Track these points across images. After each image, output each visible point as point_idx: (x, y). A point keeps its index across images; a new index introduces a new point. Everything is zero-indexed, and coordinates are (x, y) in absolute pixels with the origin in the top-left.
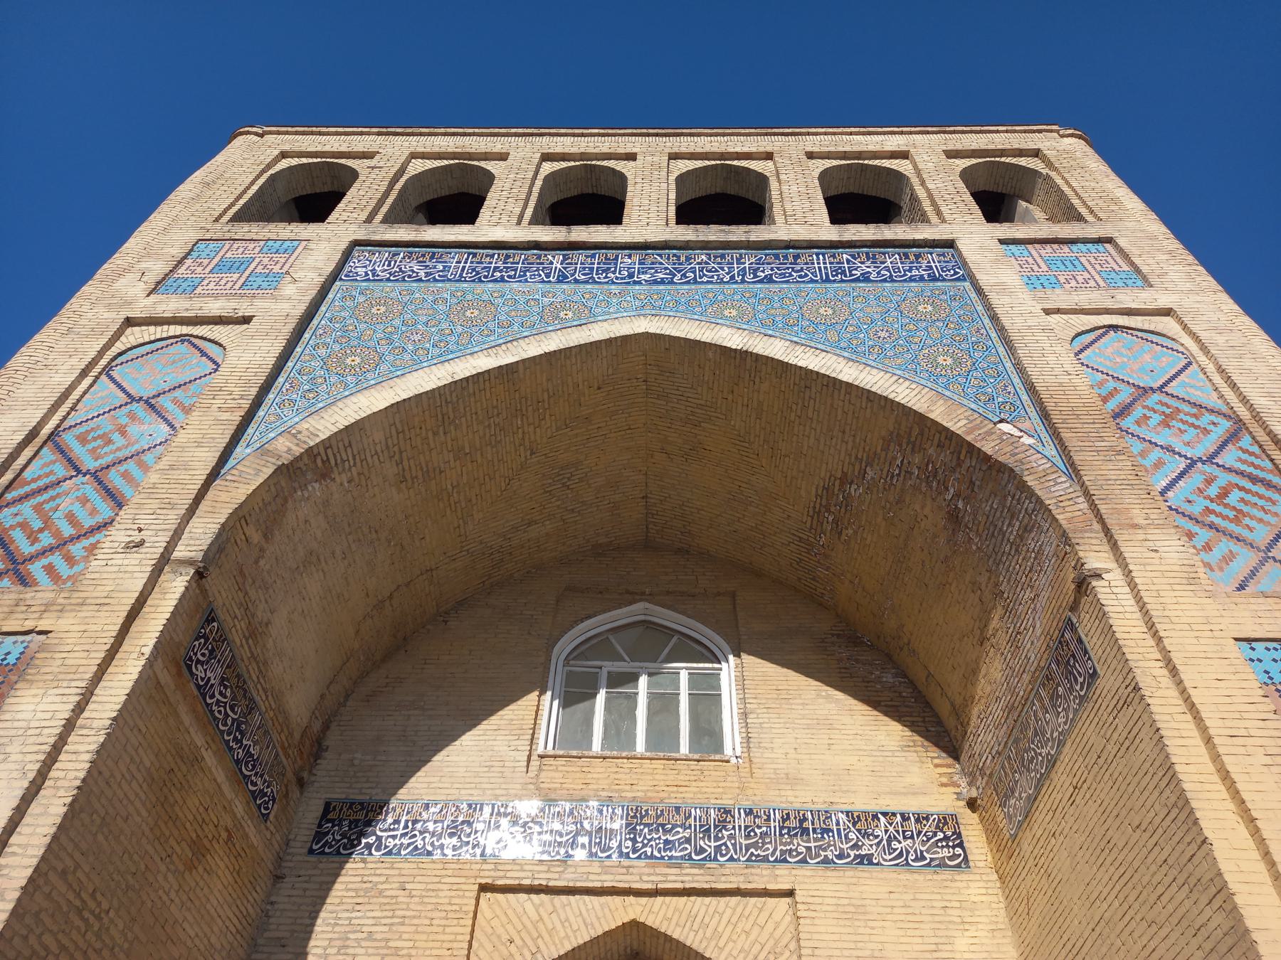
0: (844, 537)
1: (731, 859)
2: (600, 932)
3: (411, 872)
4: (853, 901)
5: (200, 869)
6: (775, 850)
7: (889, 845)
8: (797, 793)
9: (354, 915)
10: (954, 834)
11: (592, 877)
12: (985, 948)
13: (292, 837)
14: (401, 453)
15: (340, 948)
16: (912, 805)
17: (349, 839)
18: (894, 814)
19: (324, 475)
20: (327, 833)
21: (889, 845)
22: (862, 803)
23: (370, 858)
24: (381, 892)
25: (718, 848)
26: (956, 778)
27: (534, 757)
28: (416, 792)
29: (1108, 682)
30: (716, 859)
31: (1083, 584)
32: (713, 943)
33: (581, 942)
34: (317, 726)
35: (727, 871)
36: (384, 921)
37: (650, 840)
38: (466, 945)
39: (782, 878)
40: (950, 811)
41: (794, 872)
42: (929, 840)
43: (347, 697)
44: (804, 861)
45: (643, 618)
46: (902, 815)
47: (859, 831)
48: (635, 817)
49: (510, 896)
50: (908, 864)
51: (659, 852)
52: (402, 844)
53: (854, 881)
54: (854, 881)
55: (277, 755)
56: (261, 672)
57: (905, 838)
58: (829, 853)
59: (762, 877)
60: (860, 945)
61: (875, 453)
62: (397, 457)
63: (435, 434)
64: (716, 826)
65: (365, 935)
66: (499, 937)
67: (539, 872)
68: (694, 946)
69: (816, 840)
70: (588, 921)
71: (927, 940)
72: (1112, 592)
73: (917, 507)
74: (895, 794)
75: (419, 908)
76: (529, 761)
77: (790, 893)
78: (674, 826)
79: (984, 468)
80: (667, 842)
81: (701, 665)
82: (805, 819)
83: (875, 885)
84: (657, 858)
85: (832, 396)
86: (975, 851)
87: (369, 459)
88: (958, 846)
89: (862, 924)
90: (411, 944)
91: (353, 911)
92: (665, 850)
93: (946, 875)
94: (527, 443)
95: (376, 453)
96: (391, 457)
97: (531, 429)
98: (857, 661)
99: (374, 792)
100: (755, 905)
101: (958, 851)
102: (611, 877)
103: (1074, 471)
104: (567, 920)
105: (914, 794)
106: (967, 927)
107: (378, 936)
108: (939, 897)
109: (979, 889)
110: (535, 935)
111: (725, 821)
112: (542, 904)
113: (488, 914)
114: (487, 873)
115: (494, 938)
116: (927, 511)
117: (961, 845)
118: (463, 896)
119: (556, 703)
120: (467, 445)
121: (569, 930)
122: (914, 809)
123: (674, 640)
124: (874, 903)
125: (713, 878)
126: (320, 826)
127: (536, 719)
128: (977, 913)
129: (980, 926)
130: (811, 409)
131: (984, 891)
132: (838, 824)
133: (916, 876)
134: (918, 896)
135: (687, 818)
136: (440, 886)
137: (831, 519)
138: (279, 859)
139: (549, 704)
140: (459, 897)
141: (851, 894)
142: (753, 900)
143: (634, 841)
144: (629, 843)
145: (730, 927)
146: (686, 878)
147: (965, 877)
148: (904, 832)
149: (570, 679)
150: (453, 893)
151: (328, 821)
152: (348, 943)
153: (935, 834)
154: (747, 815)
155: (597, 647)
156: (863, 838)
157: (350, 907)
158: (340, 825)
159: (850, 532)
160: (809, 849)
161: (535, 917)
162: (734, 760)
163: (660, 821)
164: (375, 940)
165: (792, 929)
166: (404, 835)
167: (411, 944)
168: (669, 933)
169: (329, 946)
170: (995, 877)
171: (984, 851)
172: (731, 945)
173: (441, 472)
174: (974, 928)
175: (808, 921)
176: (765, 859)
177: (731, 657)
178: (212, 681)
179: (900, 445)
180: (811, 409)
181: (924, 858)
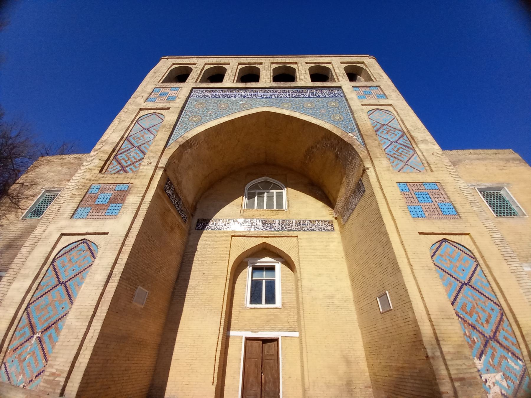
16: (323, 219)
22: (313, 218)
29: (367, 192)
31: (364, 171)
34: (194, 204)
39: (295, 234)
72: (371, 173)
77: (297, 237)
83: (313, 235)
93: (329, 232)
103: (365, 145)
109: (336, 235)
155: (255, 187)
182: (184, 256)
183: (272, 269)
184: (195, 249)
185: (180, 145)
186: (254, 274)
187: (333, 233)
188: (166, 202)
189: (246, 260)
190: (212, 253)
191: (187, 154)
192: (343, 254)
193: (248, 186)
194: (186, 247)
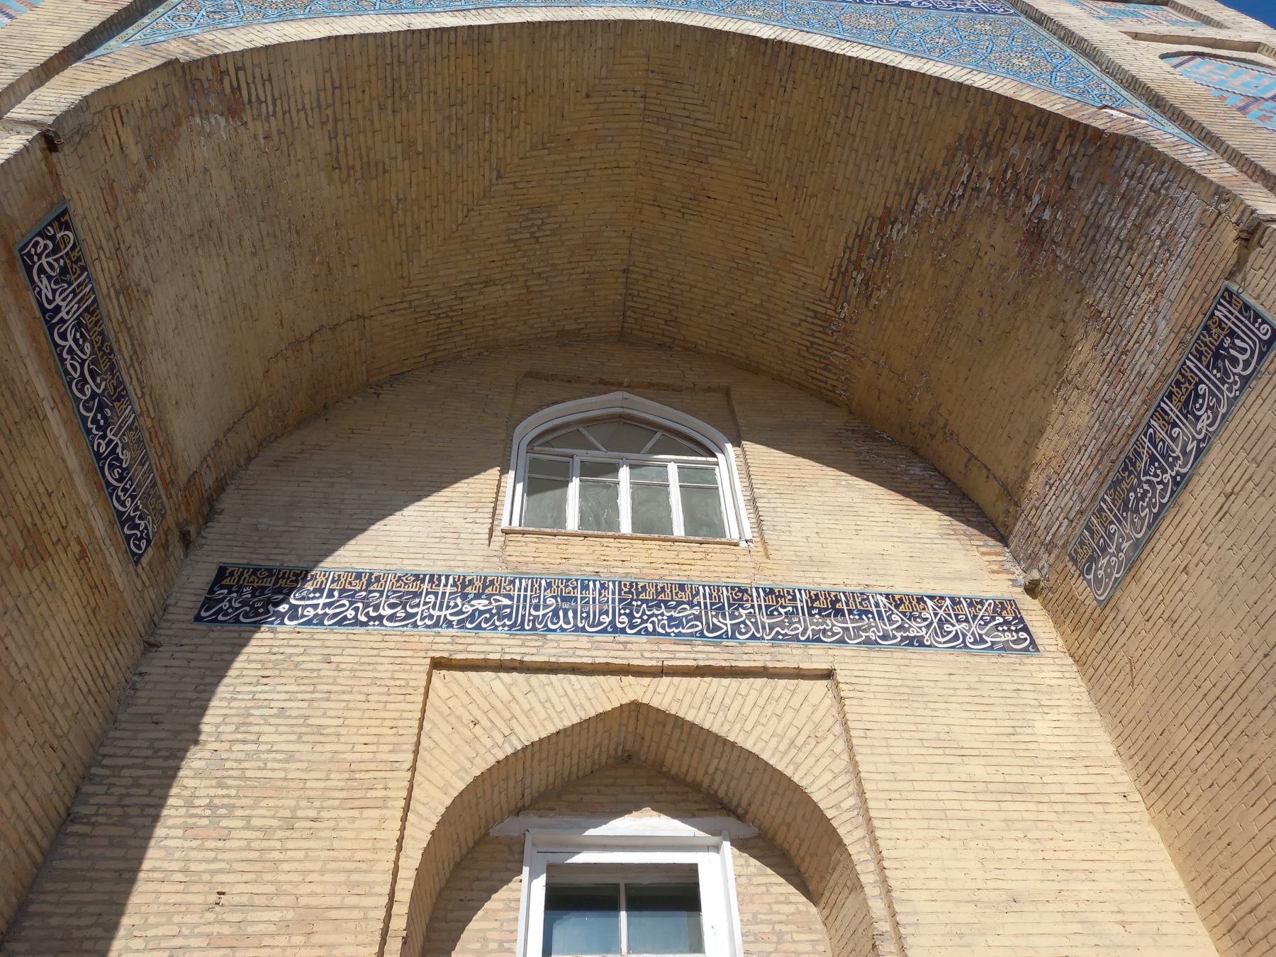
0: (874, 302)
1: (753, 637)
2: (592, 714)
3: (339, 644)
4: (907, 682)
5: (36, 572)
6: (805, 629)
7: (941, 628)
8: (825, 575)
9: (259, 688)
10: (1014, 619)
11: (578, 652)
12: (1071, 732)
13: (170, 602)
14: (336, 121)
15: (238, 726)
16: (964, 590)
17: (252, 607)
18: (942, 598)
19: (233, 111)
20: (222, 600)
21: (941, 628)
22: (901, 587)
23: (280, 628)
24: (297, 664)
25: (735, 627)
26: (1008, 566)
27: (497, 532)
28: (344, 560)
30: (733, 637)
32: (737, 727)
33: (568, 724)
34: (209, 480)
35: (750, 650)
36: (300, 696)
37: (650, 617)
38: (416, 724)
39: (818, 658)
40: (1007, 596)
41: (831, 652)
42: (986, 624)
43: (249, 459)
44: (842, 641)
45: (619, 410)
46: (952, 599)
47: (904, 613)
48: (630, 592)
49: (473, 675)
50: (966, 647)
51: (663, 627)
52: (325, 614)
53: (905, 662)
54: (905, 662)
55: (154, 485)
56: (135, 352)
57: (958, 621)
58: (870, 634)
59: (792, 657)
60: (921, 727)
61: (933, 172)
62: (330, 126)
63: (382, 108)
64: (730, 605)
65: (274, 711)
66: (459, 718)
67: (510, 646)
68: (714, 729)
69: (853, 621)
70: (576, 701)
71: (1001, 723)
73: (982, 237)
74: (940, 579)
75: (350, 682)
76: (491, 535)
77: (828, 675)
78: (679, 603)
79: (1091, 151)
80: (670, 618)
81: (693, 458)
82: (838, 601)
83: (932, 666)
84: (660, 634)
85: (887, 96)
86: (1042, 635)
87: (294, 112)
88: (1021, 630)
89: (920, 705)
90: (340, 722)
91: (258, 684)
92: (670, 627)
93: (1012, 658)
94: (494, 161)
95: (304, 109)
96: (324, 123)
97: (501, 139)
98: (878, 455)
99: (286, 558)
100: (785, 687)
101: (1023, 635)
102: (605, 653)
104: (549, 700)
105: (962, 579)
106: (1046, 710)
107: (294, 713)
108: (1008, 679)
110: (508, 716)
111: (741, 599)
112: (514, 683)
113: (444, 693)
114: (441, 647)
115: (452, 720)
116: (996, 239)
117: (1025, 629)
118: (411, 671)
119: (520, 487)
120: (420, 142)
121: (551, 712)
122: (965, 594)
123: (658, 435)
124: (932, 684)
125: (733, 657)
126: (211, 591)
127: (497, 493)
128: (1056, 696)
129: (1061, 710)
130: (855, 121)
131: (1060, 675)
132: (877, 605)
133: (977, 659)
134: (983, 678)
135: (694, 596)
136: (378, 659)
137: (859, 279)
138: (153, 624)
139: (512, 488)
140: (404, 671)
141: (903, 675)
142: (783, 682)
143: (631, 616)
144: (625, 619)
145: (757, 711)
146: (699, 656)
147: (1036, 661)
148: (956, 616)
149: (534, 466)
150: (397, 667)
151: (223, 587)
152: (251, 719)
153: (993, 619)
154: (766, 594)
156: (907, 619)
157: (254, 680)
158: (240, 592)
159: (884, 292)
160: (846, 629)
161: (507, 697)
162: (743, 544)
163: (662, 597)
164: (289, 716)
165: (834, 711)
166: (325, 605)
167: (340, 722)
168: (681, 715)
169: (224, 723)
170: (1070, 661)
171: (1054, 635)
172: (759, 729)
173: (385, 171)
174: (1054, 711)
175: (855, 702)
176: (796, 638)
177: (729, 446)
178: (63, 314)
179: (970, 152)
180: (855, 121)
181: (983, 641)
182: (87, 778)
183: (675, 895)
184: (187, 734)
185: (171, 65)
186: (558, 933)
187: (1032, 661)
188: (23, 345)
189: (512, 827)
190: (291, 757)
191: (207, 141)
192: (1120, 776)
193: (528, 429)
194: (113, 720)
